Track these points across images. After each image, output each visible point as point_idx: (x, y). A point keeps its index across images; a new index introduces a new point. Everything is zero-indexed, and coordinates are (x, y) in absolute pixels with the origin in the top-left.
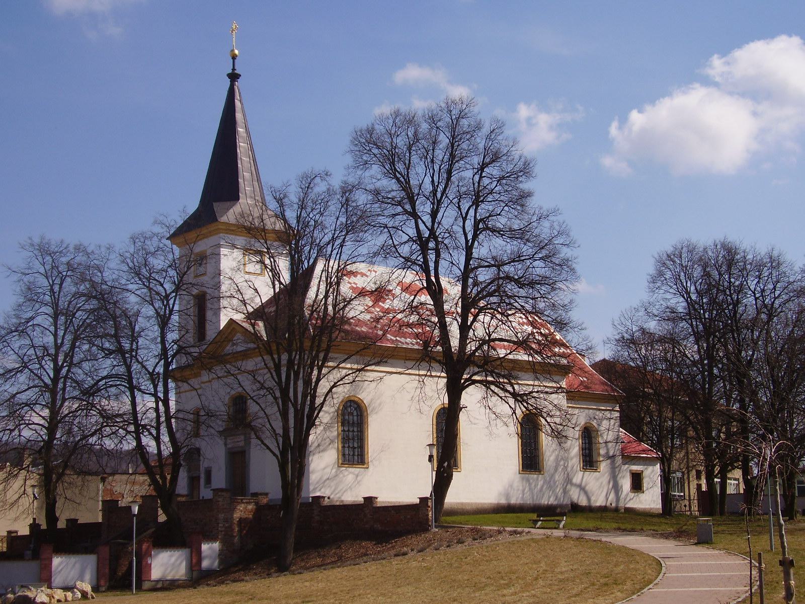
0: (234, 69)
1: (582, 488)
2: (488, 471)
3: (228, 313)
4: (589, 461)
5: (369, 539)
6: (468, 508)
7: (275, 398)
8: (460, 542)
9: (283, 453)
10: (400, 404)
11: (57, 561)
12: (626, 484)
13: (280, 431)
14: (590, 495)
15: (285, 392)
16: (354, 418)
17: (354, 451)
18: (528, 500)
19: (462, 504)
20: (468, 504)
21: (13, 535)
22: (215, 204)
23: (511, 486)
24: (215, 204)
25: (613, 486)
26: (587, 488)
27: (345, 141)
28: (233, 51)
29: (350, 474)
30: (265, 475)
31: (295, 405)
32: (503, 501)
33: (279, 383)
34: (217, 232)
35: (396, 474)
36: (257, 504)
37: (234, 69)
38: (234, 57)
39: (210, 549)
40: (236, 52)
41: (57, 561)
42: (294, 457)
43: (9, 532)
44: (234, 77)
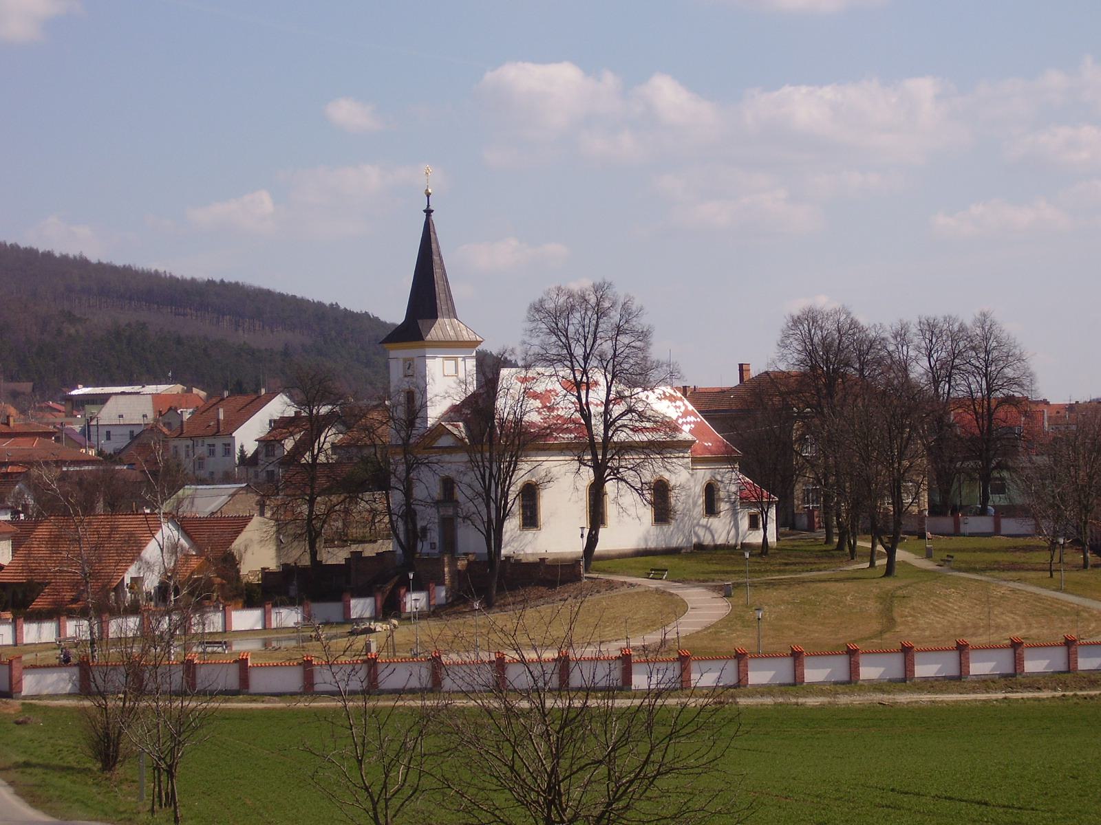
0: (428, 206)
1: (707, 528)
2: (630, 526)
3: (435, 412)
4: (711, 509)
5: (544, 586)
6: (613, 553)
7: (483, 499)
8: (598, 592)
9: (488, 532)
10: (563, 485)
11: (353, 602)
12: (744, 523)
13: (485, 519)
14: (714, 532)
15: (488, 491)
16: (530, 494)
17: (531, 520)
18: (663, 545)
19: (608, 551)
20: (612, 551)
21: (267, 571)
22: (420, 322)
23: (648, 532)
24: (420, 322)
25: (734, 524)
26: (712, 528)
27: (523, 312)
28: (427, 190)
29: (530, 534)
30: (471, 540)
31: (496, 503)
32: (642, 546)
33: (484, 488)
34: (424, 347)
35: (558, 533)
36: (468, 560)
37: (428, 206)
38: (428, 195)
39: (441, 593)
40: (430, 191)
41: (353, 602)
42: (494, 532)
43: (263, 569)
44: (428, 212)
